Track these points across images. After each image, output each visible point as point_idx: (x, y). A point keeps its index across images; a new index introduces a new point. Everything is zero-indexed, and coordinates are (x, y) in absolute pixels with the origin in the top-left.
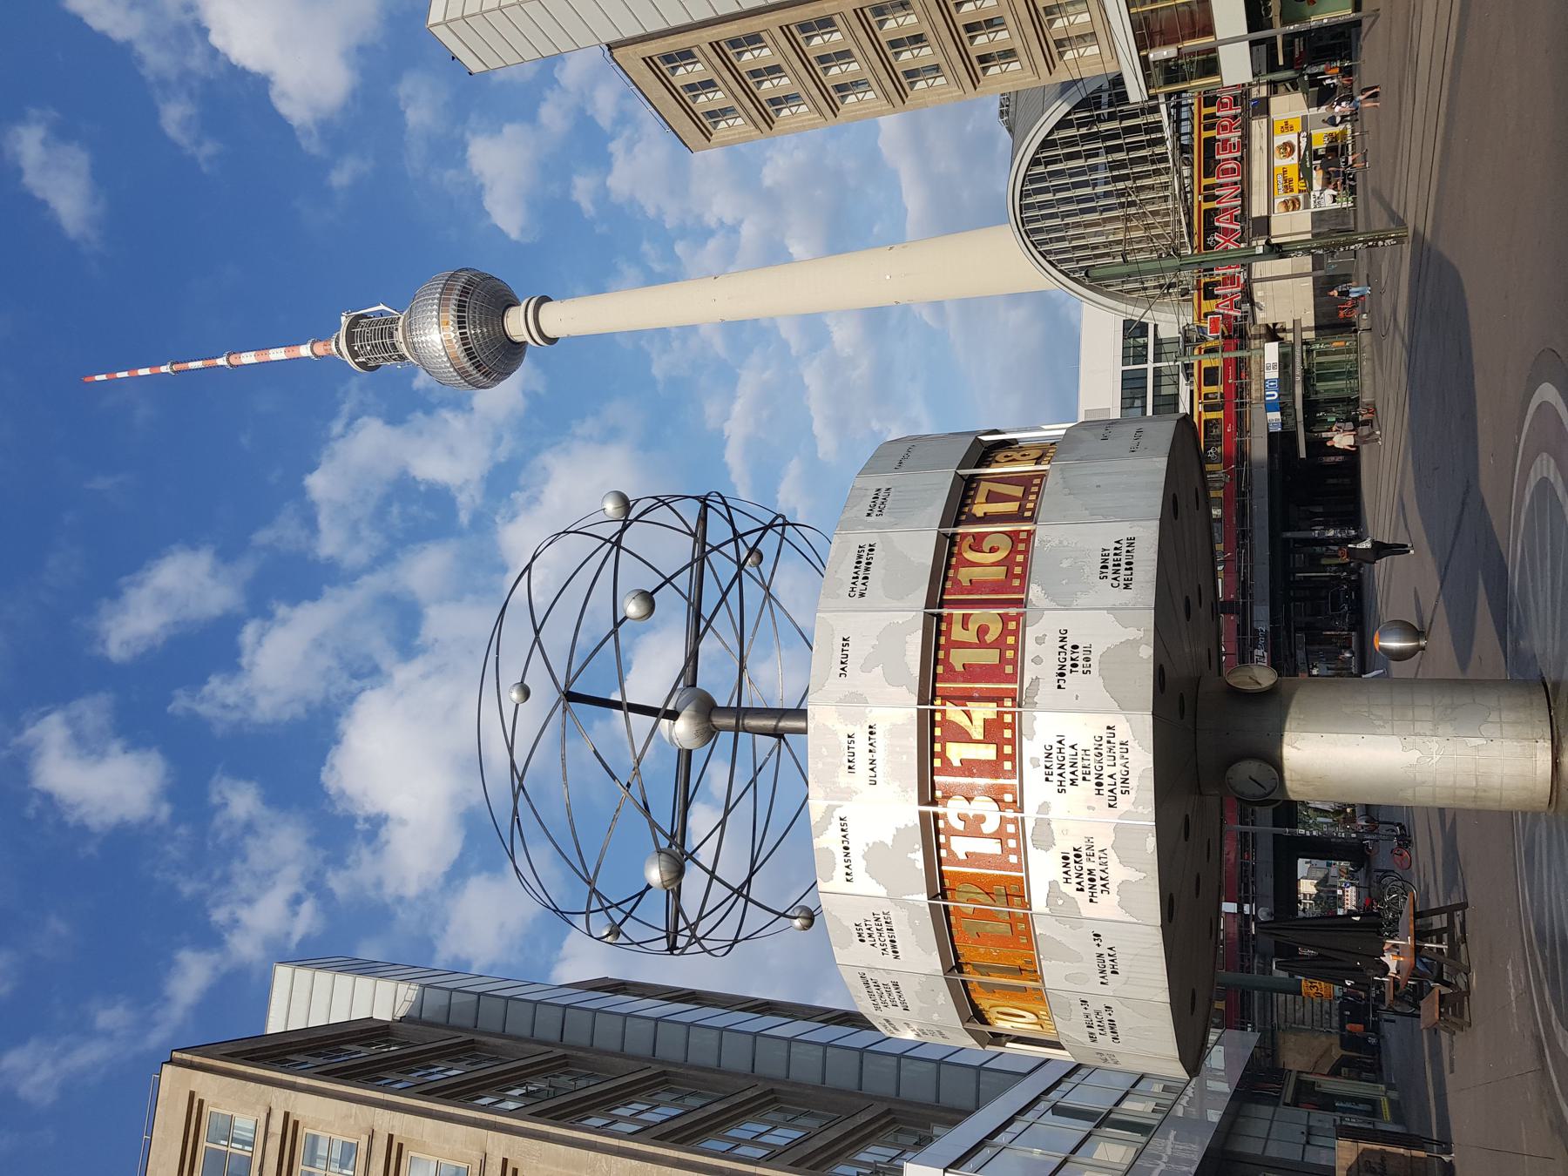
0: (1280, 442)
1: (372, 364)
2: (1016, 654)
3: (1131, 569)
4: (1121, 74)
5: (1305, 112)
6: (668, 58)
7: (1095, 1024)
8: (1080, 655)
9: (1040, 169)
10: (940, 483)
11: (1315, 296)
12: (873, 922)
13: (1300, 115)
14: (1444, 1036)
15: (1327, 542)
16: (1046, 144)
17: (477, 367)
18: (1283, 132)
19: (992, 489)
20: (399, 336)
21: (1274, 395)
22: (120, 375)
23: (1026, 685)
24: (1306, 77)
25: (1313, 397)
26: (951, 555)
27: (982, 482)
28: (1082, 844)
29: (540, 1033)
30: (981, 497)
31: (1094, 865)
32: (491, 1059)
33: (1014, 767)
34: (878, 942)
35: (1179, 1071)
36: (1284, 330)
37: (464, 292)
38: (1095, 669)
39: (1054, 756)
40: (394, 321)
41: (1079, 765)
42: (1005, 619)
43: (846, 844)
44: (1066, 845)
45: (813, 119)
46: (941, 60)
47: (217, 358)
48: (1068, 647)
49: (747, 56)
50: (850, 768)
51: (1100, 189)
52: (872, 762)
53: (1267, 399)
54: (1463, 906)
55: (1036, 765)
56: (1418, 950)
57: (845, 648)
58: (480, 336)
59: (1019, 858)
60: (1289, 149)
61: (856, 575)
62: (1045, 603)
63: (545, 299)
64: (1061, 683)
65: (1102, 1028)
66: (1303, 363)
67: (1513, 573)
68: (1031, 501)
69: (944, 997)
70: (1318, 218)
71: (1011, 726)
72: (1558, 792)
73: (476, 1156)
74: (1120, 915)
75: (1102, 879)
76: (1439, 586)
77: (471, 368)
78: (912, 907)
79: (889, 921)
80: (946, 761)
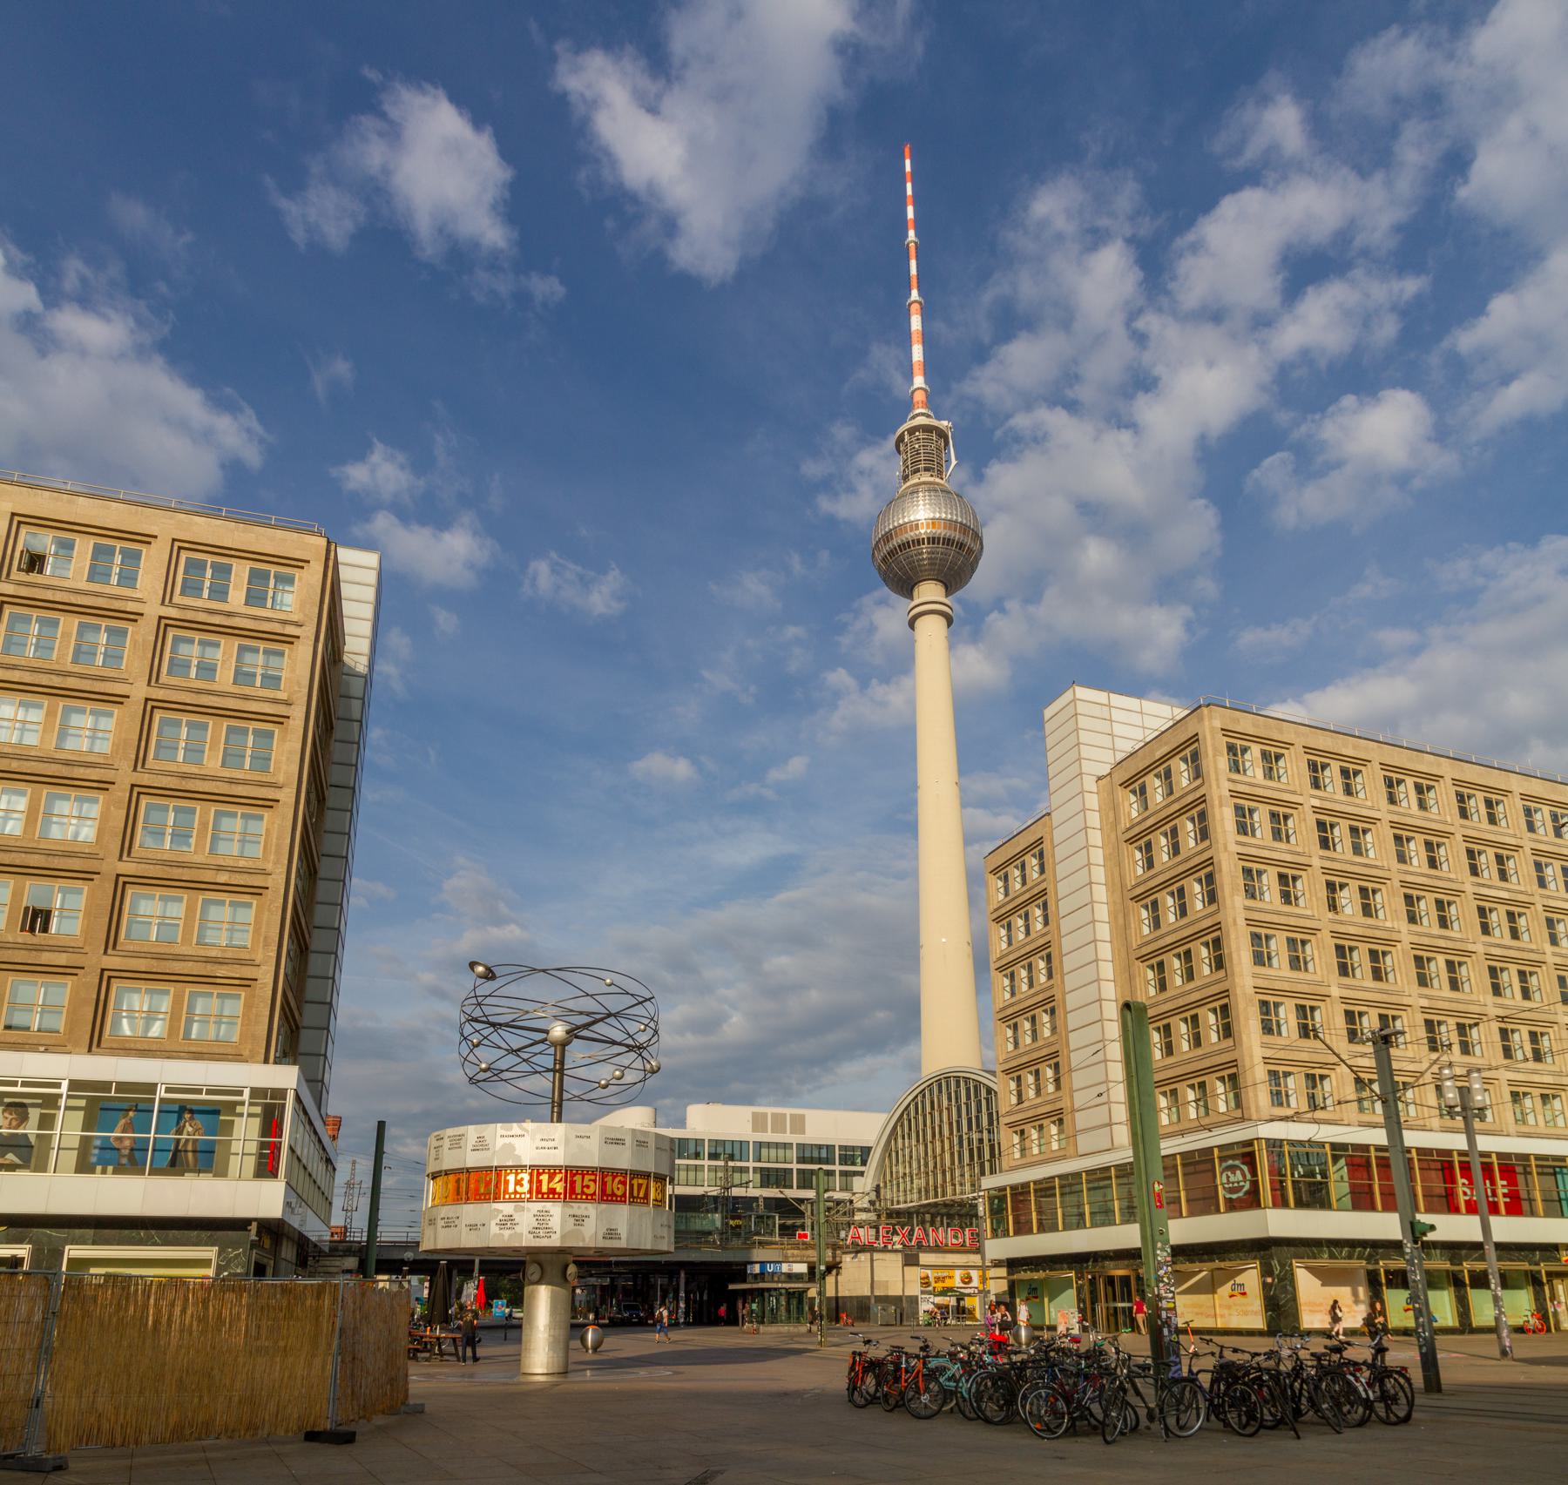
5: (993, 1292)
8: (581, 1222)
11: (857, 1297)
20: (926, 477)
37: (961, 546)
40: (940, 474)
63: (949, 620)
70: (914, 1300)
73: (281, 779)
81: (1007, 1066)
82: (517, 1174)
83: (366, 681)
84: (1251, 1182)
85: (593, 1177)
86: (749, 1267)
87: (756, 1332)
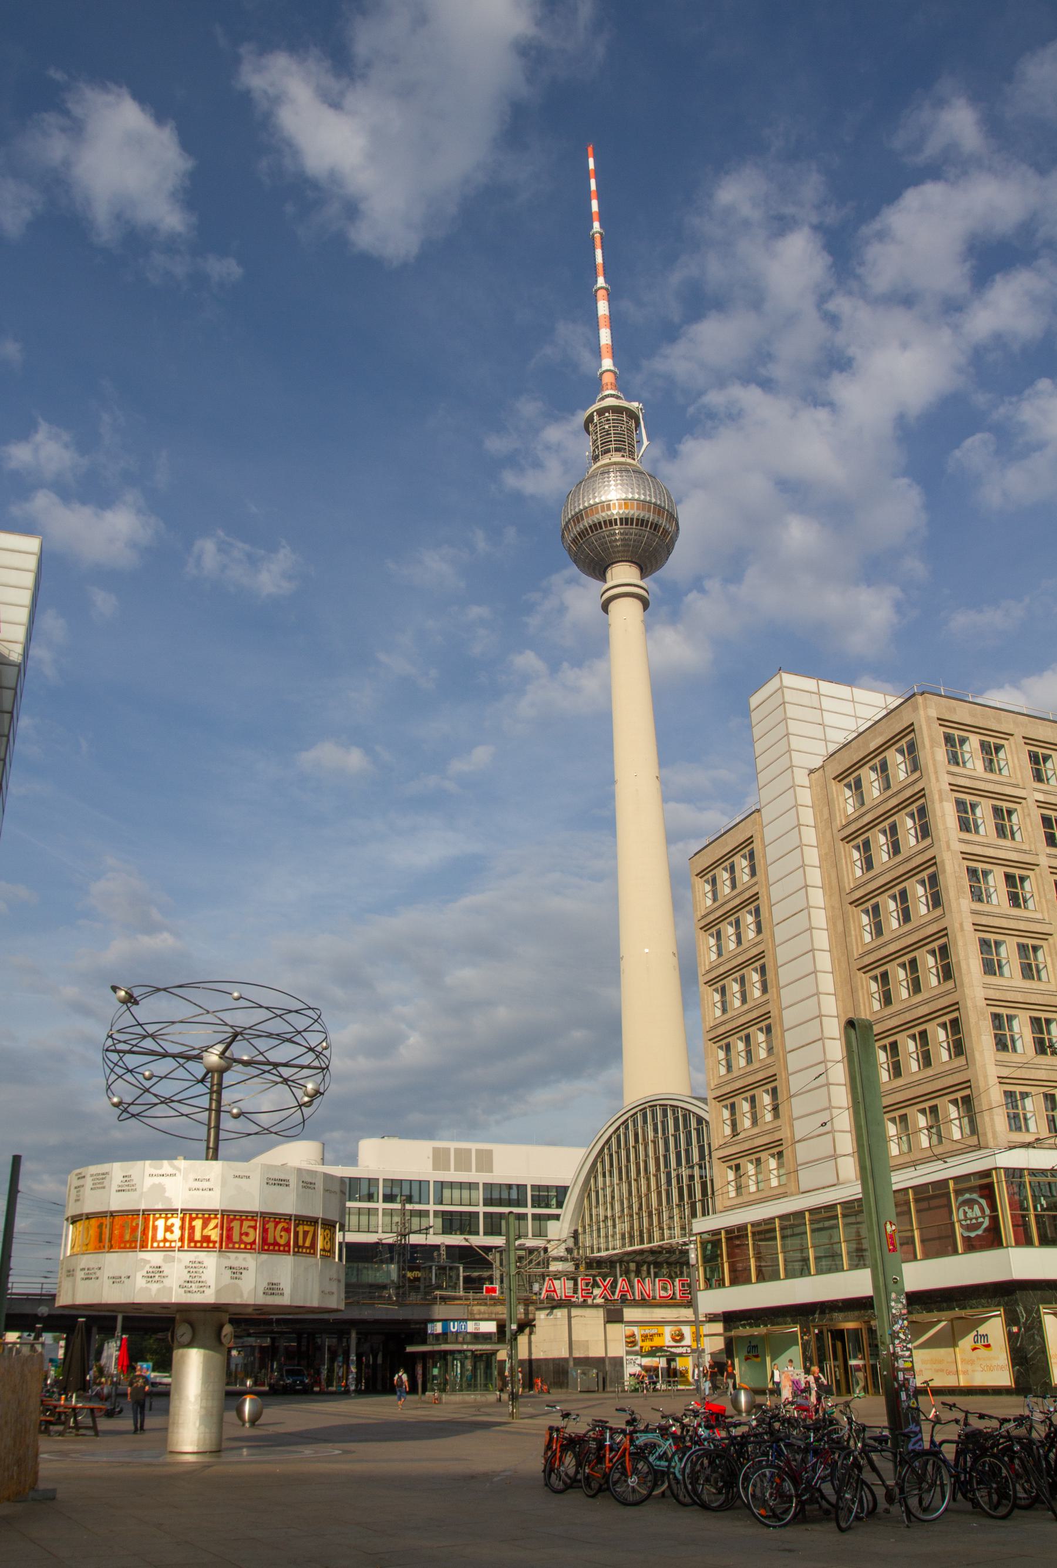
1: (591, 429)
5: (708, 1351)
8: (238, 1275)
11: (554, 1359)
17: (582, 532)
20: (617, 458)
22: (593, 182)
31: (157, 1278)
37: (656, 527)
40: (631, 454)
45: (705, 965)
47: (605, 277)
58: (613, 538)
60: (678, 1338)
63: (645, 604)
70: (618, 1362)
77: (582, 526)
82: (167, 1219)
83: (19, 671)
84: (990, 1217)
86: (429, 1326)
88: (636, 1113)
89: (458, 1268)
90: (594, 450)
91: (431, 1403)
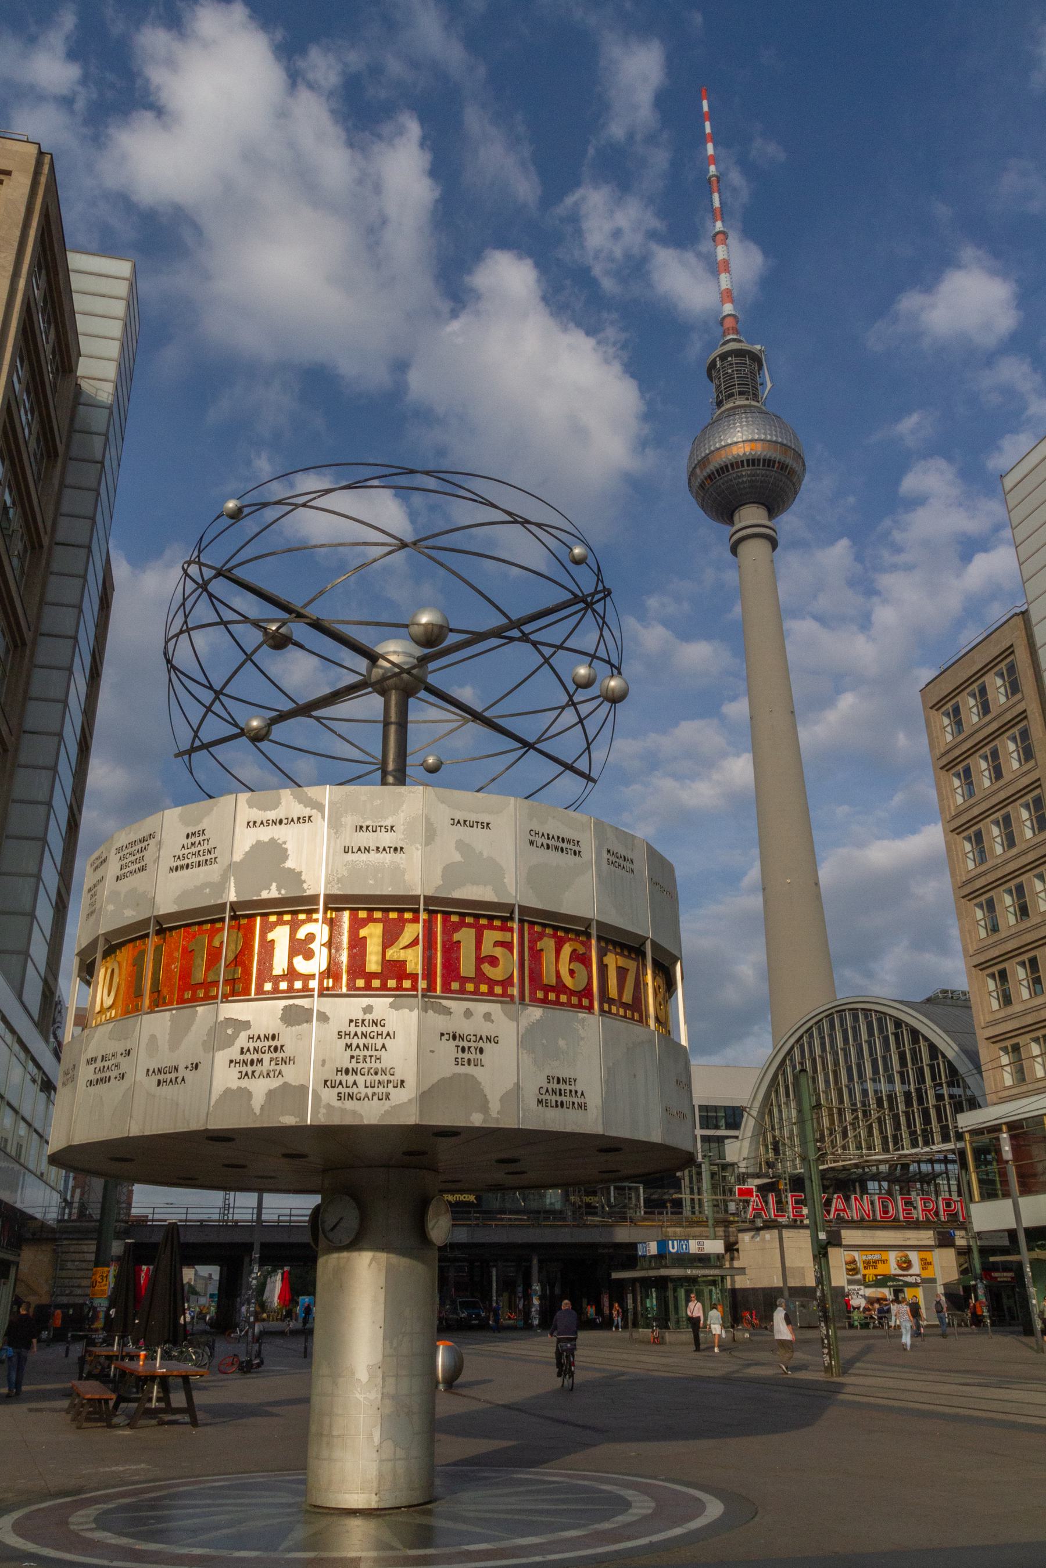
0: (628, 1255)
1: (714, 373)
2: (471, 993)
3: (557, 1106)
4: (980, 1107)
5: (940, 1281)
6: (1012, 669)
7: (106, 1064)
9: (891, 1028)
10: (640, 922)
11: (764, 1289)
12: (206, 847)
13: (937, 1277)
14: (65, 1403)
15: (527, 1297)
16: (915, 1034)
18: (921, 1260)
19: (629, 972)
20: (741, 402)
21: (673, 1247)
23: (444, 1002)
24: (972, 1283)
25: (670, 1285)
26: (567, 931)
27: (636, 963)
28: (288, 1052)
29: (63, 523)
30: (622, 962)
32: (39, 473)
33: (359, 989)
34: (186, 852)
35: (57, 1142)
36: (732, 1259)
37: (783, 466)
38: (460, 1070)
39: (375, 1028)
40: (755, 397)
41: (367, 1053)
42: (507, 982)
43: (285, 821)
44: (288, 1036)
46: (1003, 933)
48: (481, 1044)
49: (1012, 747)
50: (361, 827)
51: (870, 1086)
52: (367, 850)
53: (670, 1242)
54: (194, 1423)
55: (368, 1009)
56: (152, 1378)
57: (479, 824)
58: (740, 480)
59: (268, 992)
60: (905, 1265)
61: (551, 837)
62: (524, 1023)
64: (446, 1037)
65: (102, 1070)
66: (704, 1276)
67: (527, 1473)
68: (618, 1010)
69: (130, 915)
71: (399, 988)
72: (327, 1514)
74: (218, 1088)
75: (253, 1072)
76: (500, 1403)
78: (221, 886)
79: (208, 863)
80: (364, 923)
81: (982, 958)
82: (295, 927)
83: (111, 413)
85: (505, 936)
87: (659, 1341)
88: (821, 1020)
89: (637, 1189)
90: (718, 396)
91: (649, 1343)
